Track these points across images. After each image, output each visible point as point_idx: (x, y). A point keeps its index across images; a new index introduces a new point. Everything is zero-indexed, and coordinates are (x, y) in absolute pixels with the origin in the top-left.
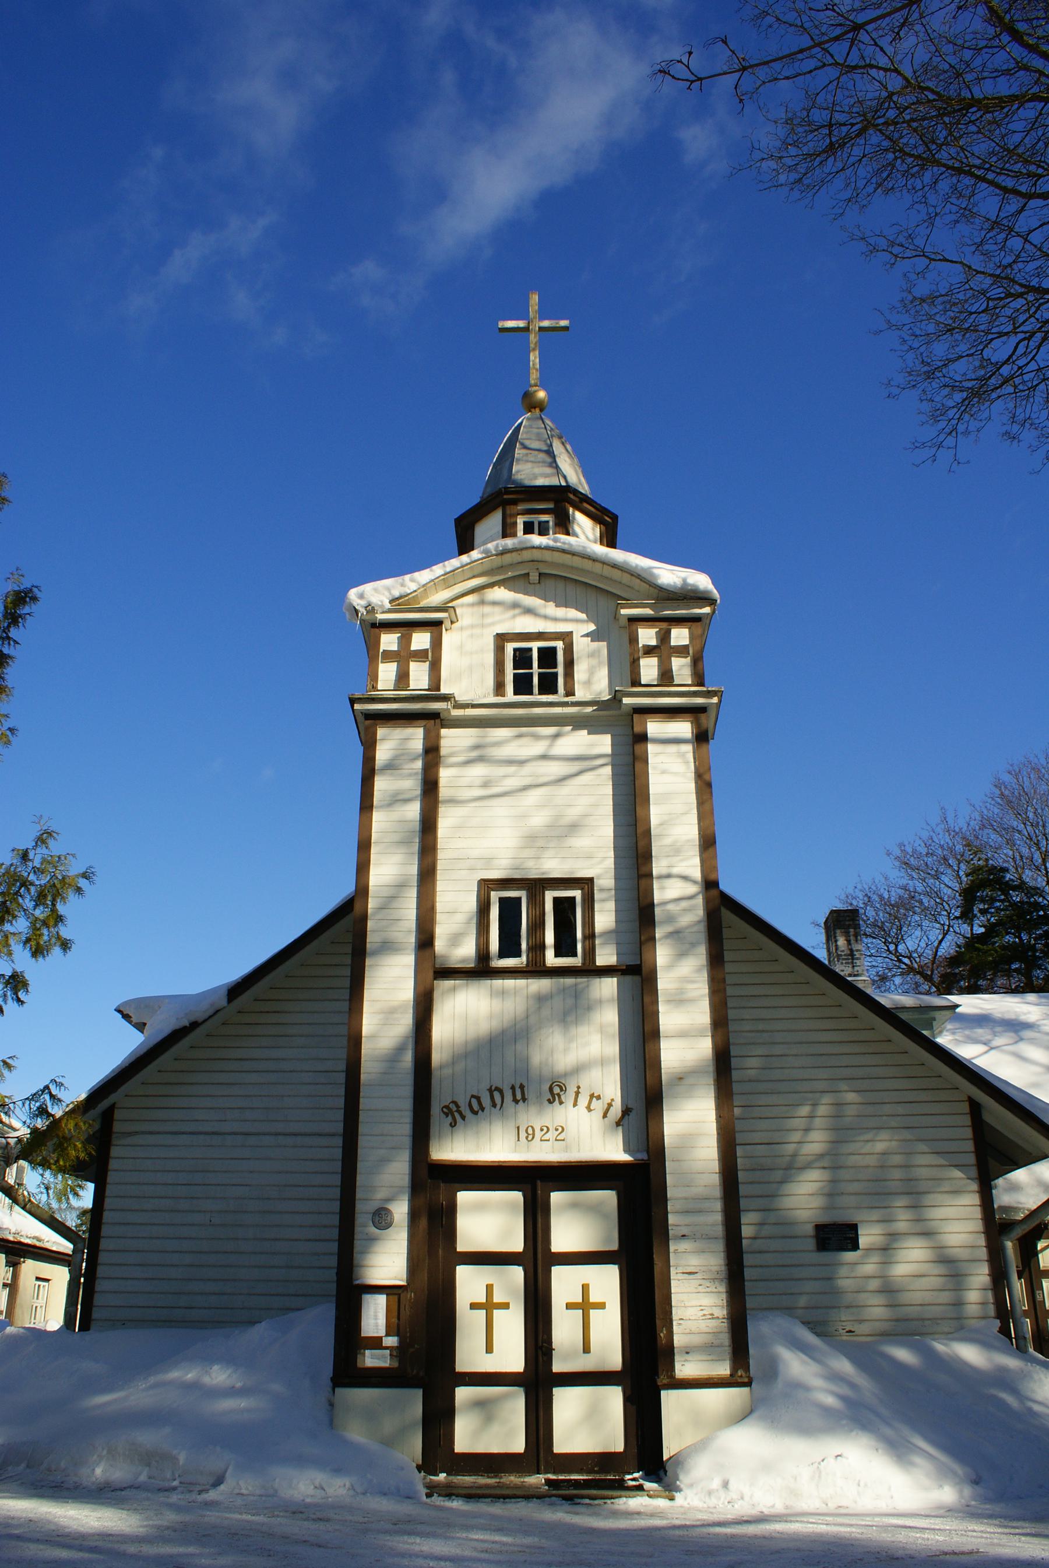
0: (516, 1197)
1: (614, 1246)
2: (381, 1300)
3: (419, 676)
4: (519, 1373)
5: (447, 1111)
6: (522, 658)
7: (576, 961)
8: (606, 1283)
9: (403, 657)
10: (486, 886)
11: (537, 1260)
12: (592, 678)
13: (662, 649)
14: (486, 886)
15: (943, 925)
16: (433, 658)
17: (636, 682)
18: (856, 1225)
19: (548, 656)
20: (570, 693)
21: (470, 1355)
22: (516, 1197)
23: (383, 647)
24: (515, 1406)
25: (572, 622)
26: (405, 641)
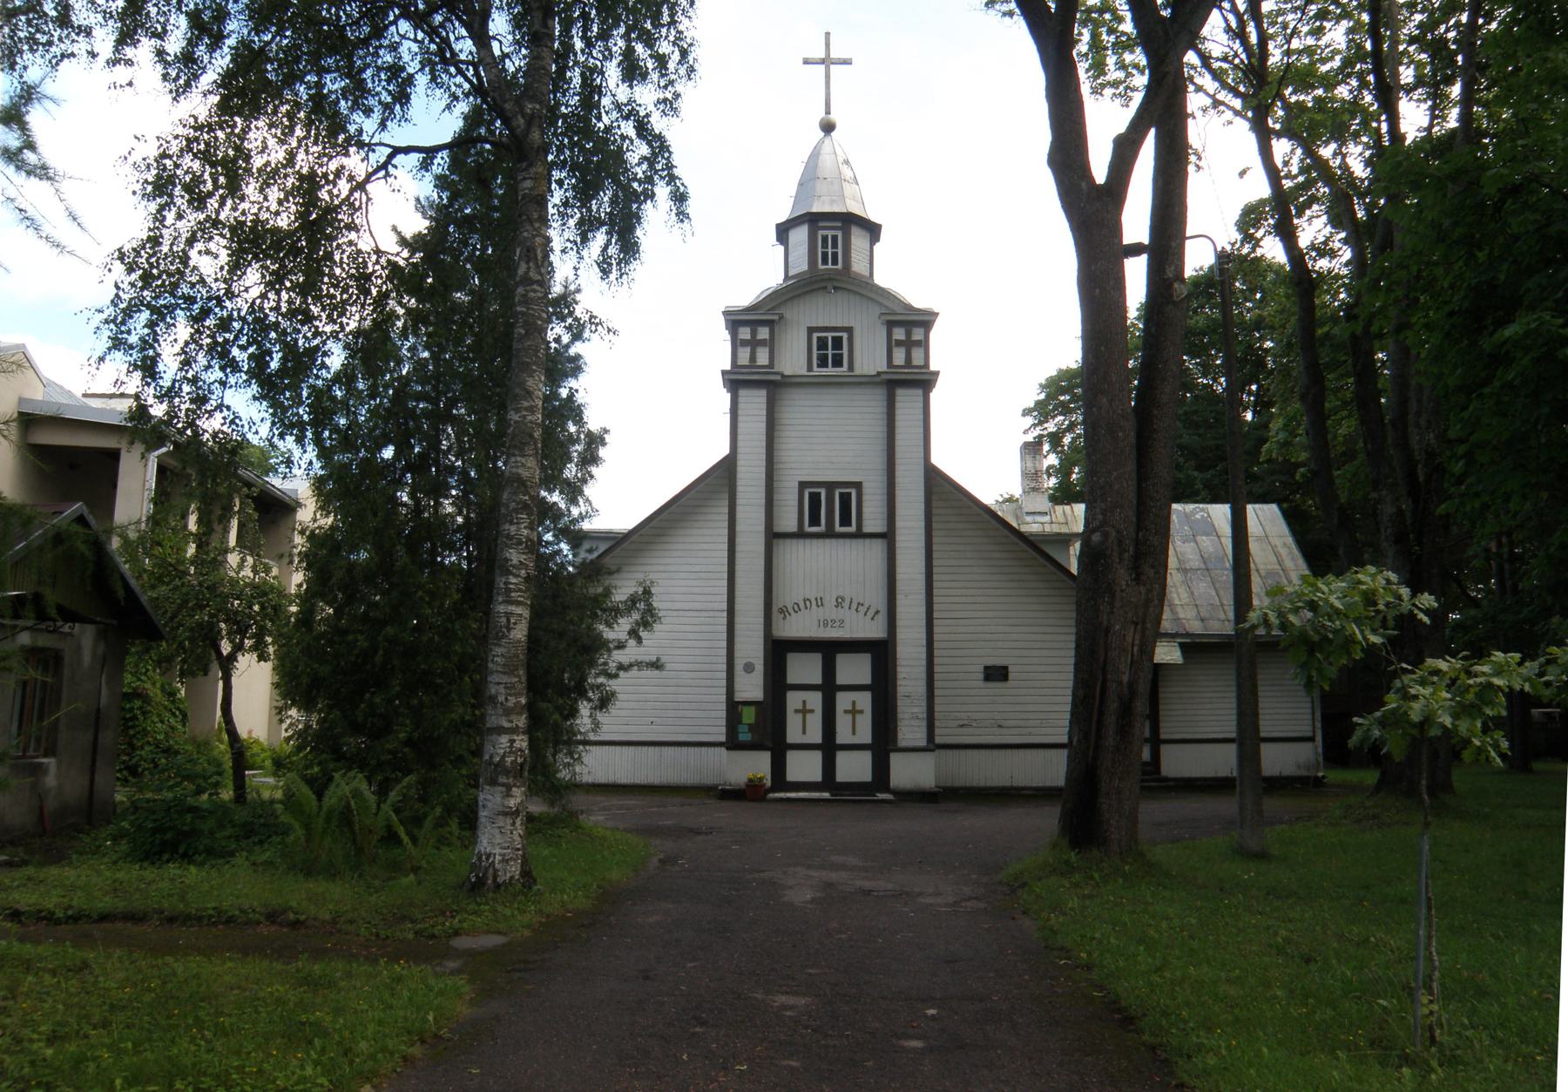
0: (763, 393)
1: (869, 682)
2: (752, 709)
5: (781, 611)
6: (822, 344)
7: (853, 529)
8: (865, 700)
10: (803, 485)
11: (829, 688)
15: (230, 294)
19: (838, 343)
20: (851, 368)
21: (793, 734)
22: (763, 393)
24: (816, 758)
26: (754, 333)
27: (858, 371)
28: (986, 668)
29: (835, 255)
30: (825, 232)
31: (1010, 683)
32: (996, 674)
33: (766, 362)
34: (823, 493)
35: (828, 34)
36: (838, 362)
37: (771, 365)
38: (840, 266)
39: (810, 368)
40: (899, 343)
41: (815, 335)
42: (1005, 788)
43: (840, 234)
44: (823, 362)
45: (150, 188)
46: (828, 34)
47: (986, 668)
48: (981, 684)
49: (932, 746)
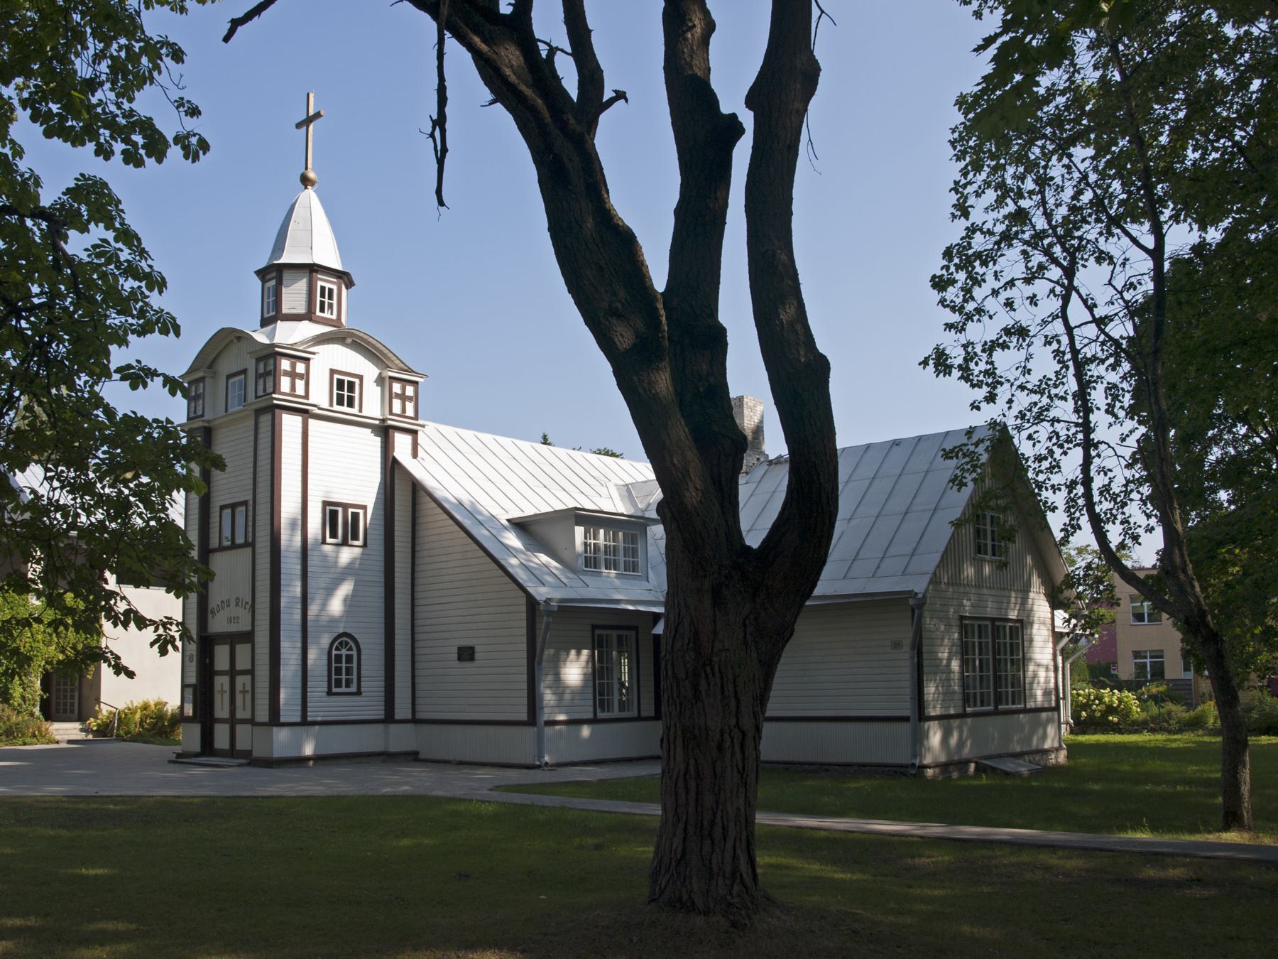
3: (300, 389)
6: (340, 382)
9: (293, 375)
10: (326, 504)
12: (372, 404)
13: (403, 398)
16: (306, 377)
17: (391, 413)
19: (351, 385)
20: (361, 410)
25: (369, 371)
28: (460, 649)
31: (477, 663)
32: (466, 654)
34: (340, 510)
35: (227, 39)
36: (351, 404)
37: (307, 396)
39: (331, 405)
40: (397, 396)
41: (336, 377)
43: (335, 288)
44: (340, 402)
45: (991, 146)
46: (227, 39)
47: (460, 649)
48: (457, 663)
49: (414, 720)
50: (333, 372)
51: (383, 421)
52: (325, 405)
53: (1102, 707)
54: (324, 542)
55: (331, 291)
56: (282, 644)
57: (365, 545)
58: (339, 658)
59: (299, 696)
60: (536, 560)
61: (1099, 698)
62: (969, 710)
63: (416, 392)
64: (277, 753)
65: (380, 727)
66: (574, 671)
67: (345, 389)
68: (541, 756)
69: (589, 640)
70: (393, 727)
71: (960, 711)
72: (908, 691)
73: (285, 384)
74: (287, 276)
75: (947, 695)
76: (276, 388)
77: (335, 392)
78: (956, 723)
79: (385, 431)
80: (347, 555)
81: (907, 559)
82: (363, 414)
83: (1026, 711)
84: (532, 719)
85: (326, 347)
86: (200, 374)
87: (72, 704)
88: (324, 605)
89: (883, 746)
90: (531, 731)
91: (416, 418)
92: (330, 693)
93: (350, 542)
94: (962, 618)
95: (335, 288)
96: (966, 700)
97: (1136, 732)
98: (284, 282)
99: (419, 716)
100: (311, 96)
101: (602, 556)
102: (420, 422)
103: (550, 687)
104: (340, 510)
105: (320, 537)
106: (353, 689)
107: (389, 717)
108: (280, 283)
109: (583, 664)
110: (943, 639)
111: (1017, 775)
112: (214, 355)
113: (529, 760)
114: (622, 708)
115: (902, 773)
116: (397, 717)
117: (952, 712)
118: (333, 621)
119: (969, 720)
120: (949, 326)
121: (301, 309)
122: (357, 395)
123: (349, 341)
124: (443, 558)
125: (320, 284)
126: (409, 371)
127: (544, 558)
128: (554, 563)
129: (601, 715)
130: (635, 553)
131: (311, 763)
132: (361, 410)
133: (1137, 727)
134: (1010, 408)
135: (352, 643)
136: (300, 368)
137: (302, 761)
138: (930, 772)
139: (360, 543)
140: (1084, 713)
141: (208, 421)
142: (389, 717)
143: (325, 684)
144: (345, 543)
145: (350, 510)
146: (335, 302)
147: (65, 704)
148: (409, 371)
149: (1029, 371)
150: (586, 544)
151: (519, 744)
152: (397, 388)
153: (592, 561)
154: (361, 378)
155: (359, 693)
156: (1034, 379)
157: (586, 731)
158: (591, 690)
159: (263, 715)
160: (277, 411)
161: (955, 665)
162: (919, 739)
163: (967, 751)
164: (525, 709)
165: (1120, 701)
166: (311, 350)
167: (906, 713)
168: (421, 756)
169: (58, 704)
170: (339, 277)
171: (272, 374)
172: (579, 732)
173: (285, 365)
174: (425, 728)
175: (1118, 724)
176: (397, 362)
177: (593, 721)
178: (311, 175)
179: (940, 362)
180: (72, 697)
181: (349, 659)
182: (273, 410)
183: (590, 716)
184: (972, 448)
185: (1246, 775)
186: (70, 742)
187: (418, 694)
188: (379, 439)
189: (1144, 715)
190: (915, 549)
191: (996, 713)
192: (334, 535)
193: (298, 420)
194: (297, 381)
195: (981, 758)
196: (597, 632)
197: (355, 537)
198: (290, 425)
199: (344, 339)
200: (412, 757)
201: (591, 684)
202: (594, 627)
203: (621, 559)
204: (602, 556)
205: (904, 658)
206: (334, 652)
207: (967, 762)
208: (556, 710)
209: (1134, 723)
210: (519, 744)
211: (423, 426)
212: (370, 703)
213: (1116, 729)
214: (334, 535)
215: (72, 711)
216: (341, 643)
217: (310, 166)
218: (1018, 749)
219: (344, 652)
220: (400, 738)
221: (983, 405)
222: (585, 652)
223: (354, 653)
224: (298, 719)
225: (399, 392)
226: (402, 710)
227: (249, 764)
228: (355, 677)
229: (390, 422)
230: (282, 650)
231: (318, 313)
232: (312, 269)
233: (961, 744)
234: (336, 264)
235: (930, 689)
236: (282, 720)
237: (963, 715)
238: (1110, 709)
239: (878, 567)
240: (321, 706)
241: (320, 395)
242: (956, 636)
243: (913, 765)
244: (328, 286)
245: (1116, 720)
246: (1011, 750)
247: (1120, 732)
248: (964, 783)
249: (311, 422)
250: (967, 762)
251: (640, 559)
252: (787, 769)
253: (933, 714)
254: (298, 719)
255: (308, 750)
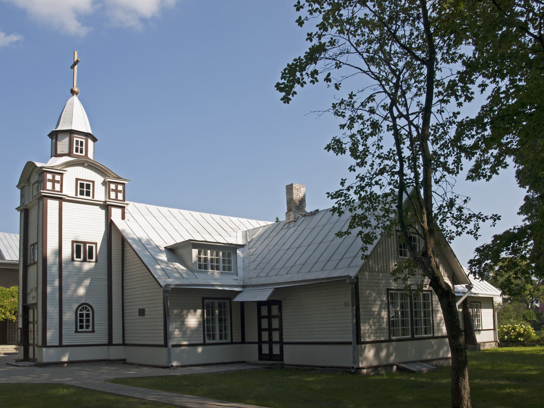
3: (57, 187)
4: (273, 305)
9: (53, 181)
10: (73, 242)
12: (100, 194)
13: (116, 191)
14: (73, 242)
16: (61, 182)
17: (109, 198)
18: (281, 301)
19: (88, 186)
20: (93, 197)
23: (48, 178)
25: (98, 179)
27: (95, 199)
28: (139, 310)
29: (77, 144)
30: (78, 139)
32: (142, 312)
33: (59, 190)
34: (82, 245)
37: (61, 191)
38: (83, 154)
39: (76, 195)
40: (113, 190)
41: (79, 182)
42: (108, 289)
43: (84, 141)
44: (82, 193)
49: (124, 344)
50: (77, 180)
51: (105, 202)
52: (74, 195)
53: (515, 333)
54: (73, 260)
55: (82, 143)
56: (48, 309)
57: (96, 261)
58: (82, 315)
59: (58, 333)
60: (172, 266)
61: (514, 329)
62: (394, 338)
63: (124, 188)
64: (45, 360)
65: (106, 347)
66: (193, 320)
67: (85, 188)
68: (170, 362)
69: (201, 305)
70: (112, 348)
71: (387, 338)
72: (351, 328)
73: (49, 185)
74: (60, 136)
75: (379, 330)
76: (45, 188)
77: (79, 189)
78: (384, 345)
79: (106, 207)
80: (87, 266)
81: (352, 259)
82: (95, 199)
83: (434, 338)
84: (166, 345)
85: (71, 168)
86: (23, 185)
87: (15, 337)
88: (76, 290)
89: (339, 357)
90: (164, 350)
91: (124, 200)
92: (76, 331)
93: (88, 260)
94: (388, 290)
95: (84, 141)
96: (391, 332)
97: (534, 345)
98: (59, 139)
99: (126, 342)
100: (76, 53)
101: (209, 264)
102: (126, 202)
103: (178, 328)
104: (82, 245)
105: (71, 258)
106: (90, 329)
107: (110, 343)
108: (56, 140)
109: (199, 317)
110: (375, 301)
111: (419, 373)
112: (29, 175)
113: (164, 364)
114: (221, 338)
115: (349, 372)
116: (114, 343)
117: (382, 339)
118: (81, 297)
119: (394, 343)
120: (342, 126)
121: (66, 151)
122: (91, 190)
123: (86, 165)
124: (133, 267)
125: (75, 139)
126: (119, 178)
127: (178, 265)
128: (182, 267)
129: (208, 341)
130: (229, 262)
131: (66, 365)
132: (93, 197)
133: (533, 343)
134: (372, 169)
135: (89, 308)
136: (120, 188)
137: (60, 364)
138: (365, 371)
139: (94, 260)
140: (506, 337)
141: (26, 206)
142: (110, 343)
143: (74, 327)
144: (85, 260)
145: (88, 245)
146: (84, 147)
147: (12, 337)
148: (119, 178)
149: (382, 147)
150: (199, 258)
151: (159, 356)
152: (113, 186)
153: (203, 266)
154: (93, 182)
155: (93, 331)
156: (385, 151)
157: (200, 349)
158: (202, 329)
159: (40, 343)
160: (45, 198)
161: (384, 314)
162: (358, 354)
163: (392, 359)
164: (163, 339)
165: (525, 330)
166: (65, 169)
167: (350, 340)
168: (127, 361)
169: (9, 337)
170: (86, 136)
171: (42, 183)
172: (196, 350)
173: (49, 176)
174: (128, 348)
175: (524, 341)
176: (113, 174)
177: (204, 344)
178: (76, 89)
179: (336, 146)
180: (15, 334)
181: (88, 315)
182: (42, 199)
183: (202, 342)
184: (345, 192)
185: (466, 383)
186: (5, 354)
187: (126, 332)
188: (104, 211)
189: (537, 338)
190: (357, 254)
191: (413, 339)
192: (78, 256)
193: (57, 202)
194: (119, 194)
195: (400, 363)
196: (206, 301)
197: (91, 257)
198: (52, 206)
199: (84, 164)
200: (123, 362)
201: (202, 326)
202: (203, 299)
203: (221, 265)
204: (209, 264)
205: (349, 311)
206: (79, 312)
207: (391, 365)
208: (181, 339)
209: (533, 341)
210: (159, 356)
211: (127, 204)
212: (100, 336)
213: (523, 344)
214: (78, 256)
215: (15, 340)
216: (83, 308)
217: (75, 85)
218: (429, 357)
219: (85, 312)
220: (115, 353)
221: (357, 168)
222: (199, 311)
223: (91, 312)
224: (57, 344)
225: (114, 188)
226: (117, 338)
227: (35, 365)
228: (91, 324)
229: (108, 203)
230: (48, 311)
231: (74, 153)
232: (71, 132)
233: (388, 355)
234: (88, 129)
235: (365, 328)
236: (48, 344)
237: (390, 341)
238: (520, 335)
239: (338, 264)
240: (70, 337)
241: (69, 190)
242: (385, 299)
243: (353, 368)
244: (80, 140)
245: (522, 340)
246: (424, 358)
247: (525, 345)
248: (377, 377)
249: (64, 203)
250: (393, 365)
251: (232, 265)
252: (297, 369)
253: (368, 340)
254: (57, 344)
255: (65, 359)
